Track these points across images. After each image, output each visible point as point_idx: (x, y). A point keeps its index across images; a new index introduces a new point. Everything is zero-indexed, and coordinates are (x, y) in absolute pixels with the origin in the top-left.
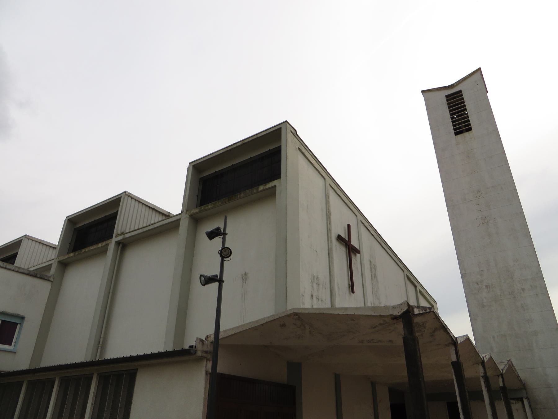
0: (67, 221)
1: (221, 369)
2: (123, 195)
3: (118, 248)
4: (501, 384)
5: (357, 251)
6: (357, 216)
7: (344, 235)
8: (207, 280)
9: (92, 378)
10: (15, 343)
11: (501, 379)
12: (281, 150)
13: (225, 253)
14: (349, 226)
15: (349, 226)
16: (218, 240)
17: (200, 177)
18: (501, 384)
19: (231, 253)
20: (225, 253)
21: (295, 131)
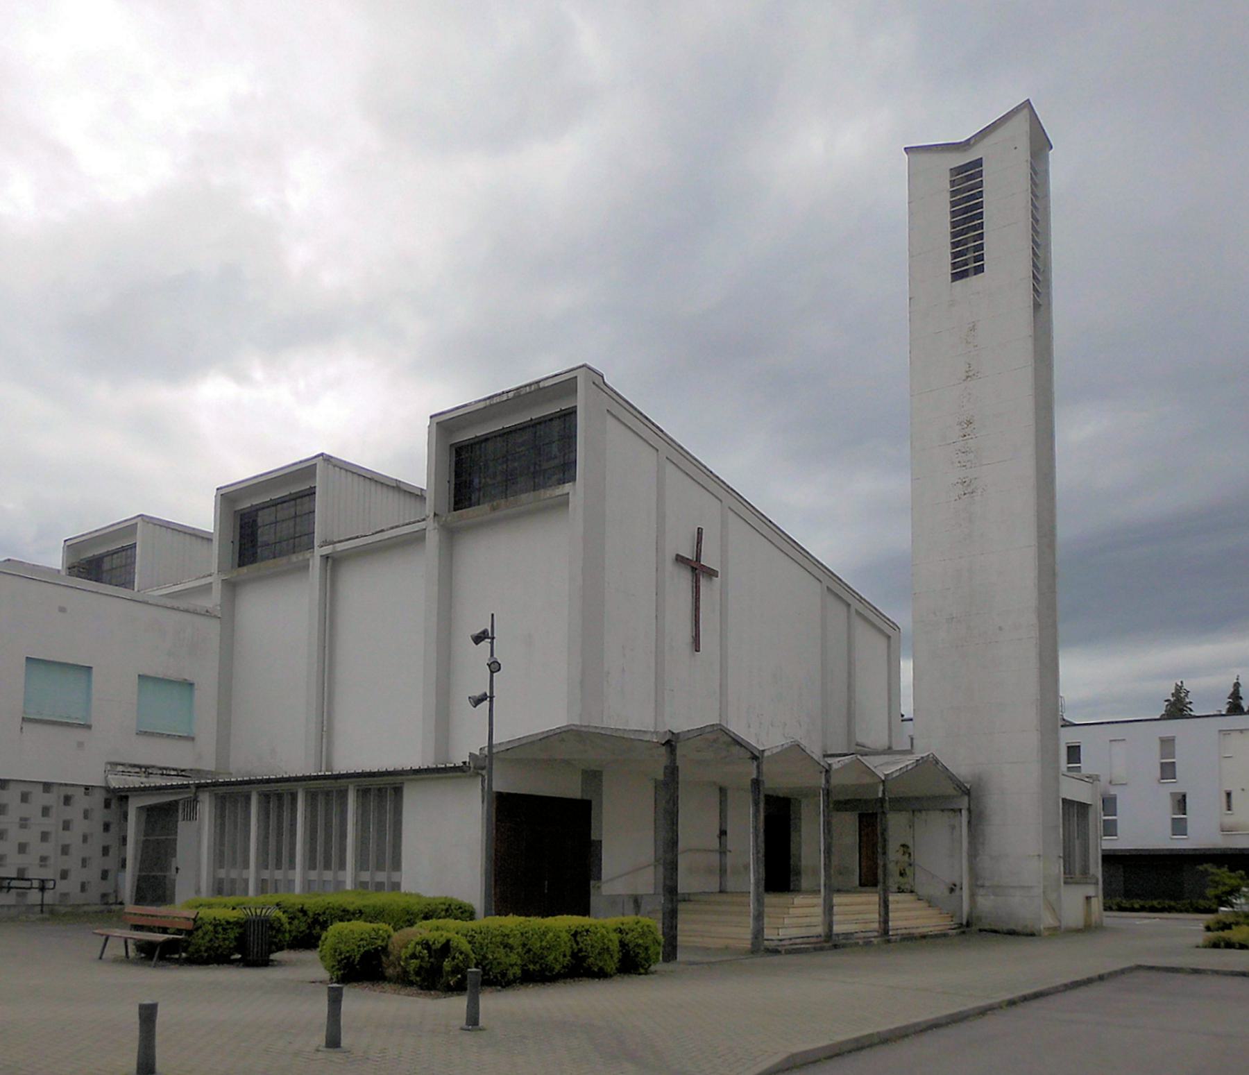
0: (219, 497)
1: (499, 786)
2: (320, 465)
3: (326, 566)
4: (880, 795)
5: (711, 573)
6: (721, 501)
7: (688, 554)
8: (477, 701)
9: (347, 791)
10: (727, 948)
11: (881, 788)
12: (576, 412)
13: (494, 667)
14: (700, 531)
15: (700, 531)
16: (486, 644)
17: (450, 443)
18: (880, 795)
19: (500, 665)
20: (494, 667)
21: (601, 378)
